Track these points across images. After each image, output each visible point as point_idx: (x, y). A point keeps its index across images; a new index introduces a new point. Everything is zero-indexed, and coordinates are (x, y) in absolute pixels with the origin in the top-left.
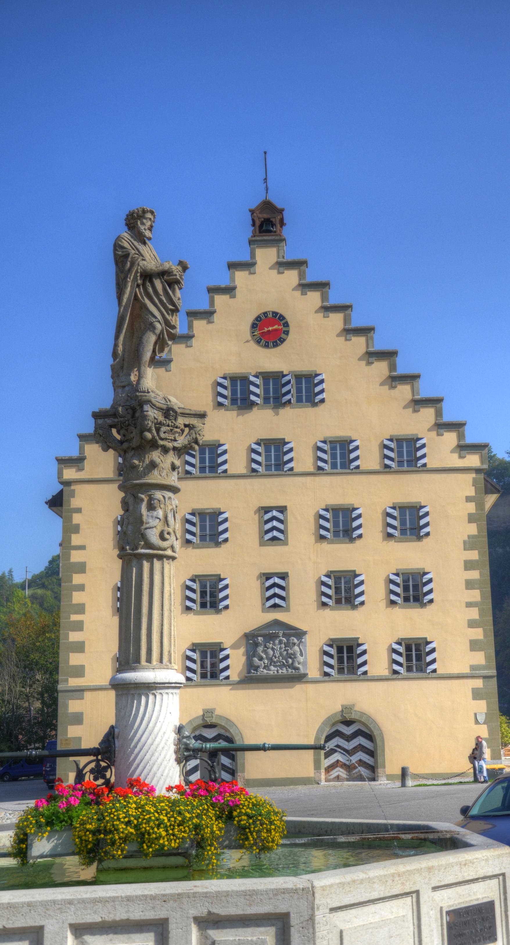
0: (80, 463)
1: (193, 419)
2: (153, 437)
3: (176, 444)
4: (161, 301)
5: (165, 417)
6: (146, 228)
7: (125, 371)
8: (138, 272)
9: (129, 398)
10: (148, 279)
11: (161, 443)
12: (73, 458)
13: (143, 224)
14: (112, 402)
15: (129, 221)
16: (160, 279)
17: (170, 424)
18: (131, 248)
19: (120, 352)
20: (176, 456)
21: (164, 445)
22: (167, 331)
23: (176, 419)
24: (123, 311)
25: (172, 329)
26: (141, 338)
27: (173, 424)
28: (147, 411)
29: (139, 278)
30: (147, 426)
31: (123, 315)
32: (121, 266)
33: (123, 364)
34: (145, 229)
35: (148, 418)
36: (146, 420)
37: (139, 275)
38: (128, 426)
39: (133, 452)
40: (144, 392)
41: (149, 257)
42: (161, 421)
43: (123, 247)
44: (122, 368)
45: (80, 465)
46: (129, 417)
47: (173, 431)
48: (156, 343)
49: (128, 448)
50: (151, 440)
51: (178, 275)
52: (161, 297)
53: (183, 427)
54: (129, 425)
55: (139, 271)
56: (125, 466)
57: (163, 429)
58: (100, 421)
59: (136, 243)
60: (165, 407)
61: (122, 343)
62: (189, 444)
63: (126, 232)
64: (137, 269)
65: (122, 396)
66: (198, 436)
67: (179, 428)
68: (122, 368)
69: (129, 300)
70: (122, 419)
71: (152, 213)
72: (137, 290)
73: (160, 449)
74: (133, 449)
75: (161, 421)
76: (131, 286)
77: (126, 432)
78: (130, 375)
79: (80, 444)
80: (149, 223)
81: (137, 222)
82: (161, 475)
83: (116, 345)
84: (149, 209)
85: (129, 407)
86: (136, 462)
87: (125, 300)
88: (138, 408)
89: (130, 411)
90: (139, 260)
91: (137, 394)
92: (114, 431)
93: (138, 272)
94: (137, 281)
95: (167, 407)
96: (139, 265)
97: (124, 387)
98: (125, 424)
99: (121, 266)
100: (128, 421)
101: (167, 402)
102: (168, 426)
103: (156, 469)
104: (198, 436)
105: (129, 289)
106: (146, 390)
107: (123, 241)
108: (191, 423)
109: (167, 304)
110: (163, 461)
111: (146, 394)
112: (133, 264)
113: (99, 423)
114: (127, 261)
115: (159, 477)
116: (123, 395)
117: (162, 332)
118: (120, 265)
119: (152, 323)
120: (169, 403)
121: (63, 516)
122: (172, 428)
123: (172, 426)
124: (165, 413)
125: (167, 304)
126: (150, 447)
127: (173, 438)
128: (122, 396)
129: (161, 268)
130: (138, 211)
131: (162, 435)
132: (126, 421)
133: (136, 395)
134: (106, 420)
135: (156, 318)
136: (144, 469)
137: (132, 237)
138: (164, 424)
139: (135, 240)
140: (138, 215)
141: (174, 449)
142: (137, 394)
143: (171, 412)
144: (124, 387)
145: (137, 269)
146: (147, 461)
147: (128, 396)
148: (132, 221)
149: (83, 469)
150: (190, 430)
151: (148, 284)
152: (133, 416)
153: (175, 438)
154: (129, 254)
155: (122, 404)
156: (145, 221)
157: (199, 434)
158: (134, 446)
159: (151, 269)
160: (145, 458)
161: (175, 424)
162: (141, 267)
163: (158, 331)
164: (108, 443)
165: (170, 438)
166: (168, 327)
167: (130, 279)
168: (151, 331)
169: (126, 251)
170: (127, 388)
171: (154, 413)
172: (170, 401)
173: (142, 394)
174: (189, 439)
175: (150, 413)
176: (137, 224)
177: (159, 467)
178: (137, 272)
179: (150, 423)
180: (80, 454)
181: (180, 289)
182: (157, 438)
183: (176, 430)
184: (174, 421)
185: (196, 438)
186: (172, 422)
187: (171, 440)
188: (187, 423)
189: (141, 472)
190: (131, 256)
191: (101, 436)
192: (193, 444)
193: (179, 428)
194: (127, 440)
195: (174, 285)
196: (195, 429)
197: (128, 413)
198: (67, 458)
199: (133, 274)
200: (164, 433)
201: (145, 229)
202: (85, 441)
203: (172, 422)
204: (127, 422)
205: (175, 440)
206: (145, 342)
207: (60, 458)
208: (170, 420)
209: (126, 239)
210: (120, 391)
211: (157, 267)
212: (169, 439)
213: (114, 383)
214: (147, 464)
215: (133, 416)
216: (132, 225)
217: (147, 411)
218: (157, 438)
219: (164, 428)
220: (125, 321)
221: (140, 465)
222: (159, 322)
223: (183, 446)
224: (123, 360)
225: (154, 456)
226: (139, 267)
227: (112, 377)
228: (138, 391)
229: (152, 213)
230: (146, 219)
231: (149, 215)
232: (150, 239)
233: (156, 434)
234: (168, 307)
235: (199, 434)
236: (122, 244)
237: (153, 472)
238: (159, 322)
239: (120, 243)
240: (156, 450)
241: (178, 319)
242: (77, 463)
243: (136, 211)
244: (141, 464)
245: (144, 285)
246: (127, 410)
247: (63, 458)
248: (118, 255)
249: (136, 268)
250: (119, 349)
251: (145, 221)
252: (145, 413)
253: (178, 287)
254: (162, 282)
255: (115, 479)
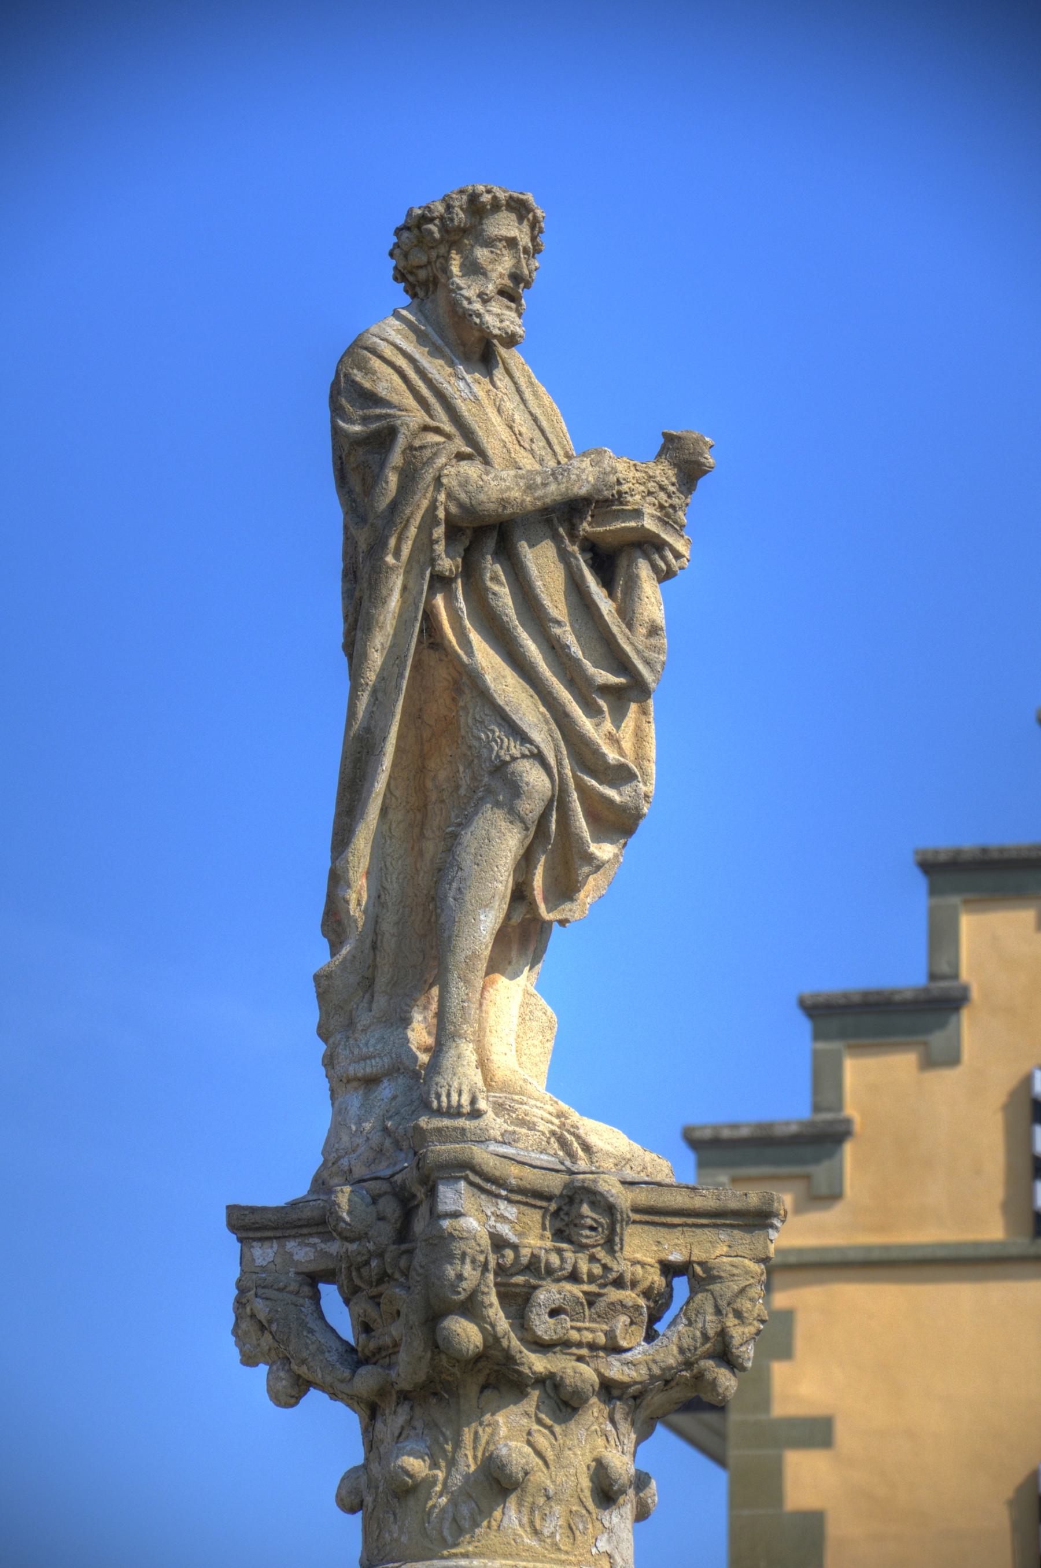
0: (817, 1160)
1: (708, 1234)
2: (492, 1340)
3: (616, 1369)
4: (554, 649)
5: (559, 1235)
6: (491, 288)
7: (381, 1001)
8: (436, 522)
9: (388, 1142)
10: (491, 544)
11: (538, 1363)
12: (780, 1131)
13: (473, 269)
14: (321, 1160)
15: (406, 255)
16: (556, 539)
17: (584, 1267)
18: (410, 401)
19: (355, 910)
20: (624, 1426)
21: (552, 1376)
22: (586, 794)
23: (610, 1244)
24: (370, 714)
25: (612, 784)
26: (455, 836)
27: (597, 1270)
28: (456, 1215)
29: (440, 548)
30: (454, 1288)
31: (368, 730)
32: (358, 489)
33: (374, 966)
34: (484, 298)
35: (458, 1247)
36: (450, 1257)
37: (439, 532)
38: (380, 1281)
39: (401, 1418)
40: (455, 1113)
41: (505, 434)
42: (535, 1258)
43: (371, 399)
44: (368, 984)
45: (820, 1171)
46: (384, 1233)
47: (601, 1304)
48: (525, 863)
49: (382, 1392)
50: (480, 1357)
51: (648, 510)
52: (557, 631)
53: (655, 1278)
54: (384, 1277)
55: (441, 514)
56: (372, 1484)
57: (548, 1294)
58: (263, 1254)
59: (437, 369)
60: (555, 1183)
61: (365, 863)
62: (688, 1365)
63: (396, 315)
64: (433, 506)
65: (360, 1131)
66: (731, 1321)
67: (634, 1284)
68: (368, 984)
69: (395, 656)
70: (353, 1247)
71: (520, 208)
72: (440, 601)
73: (535, 1394)
74: (404, 1396)
75: (535, 1258)
76: (405, 588)
77: (373, 1313)
78: (406, 1022)
79: (816, 1055)
80: (503, 266)
81: (447, 259)
82: (536, 1532)
83: (337, 879)
84: (502, 196)
85: (385, 1186)
86: (416, 1465)
87: (376, 658)
88: (420, 1193)
89: (390, 1207)
90: (441, 460)
91: (423, 1122)
92: (330, 1295)
93: (436, 522)
94: (433, 561)
95: (566, 1186)
96: (438, 481)
97: (371, 1082)
98: (365, 1271)
99: (358, 489)
100: (381, 1255)
101: (572, 1155)
102: (574, 1277)
103: (512, 1502)
104: (731, 1321)
105: (394, 602)
106: (465, 1100)
107: (376, 363)
108: (698, 1255)
109: (587, 664)
110: (550, 1455)
111: (461, 1122)
112: (409, 477)
113: (259, 1262)
114: (383, 464)
115: (529, 1541)
116: (367, 1126)
117: (559, 800)
118: (355, 481)
119: (505, 764)
120: (583, 1164)
121: (731, 1461)
122: (593, 1288)
123: (592, 1278)
124: (556, 1214)
125: (587, 664)
126: (484, 1388)
127: (602, 1339)
128: (360, 1131)
129: (553, 487)
130: (449, 208)
131: (544, 1326)
132: (371, 1254)
133: (417, 1128)
134: (291, 1245)
135: (523, 738)
136: (454, 1502)
137: (422, 338)
138: (550, 1271)
139: (436, 352)
140: (444, 229)
141: (609, 1390)
142: (423, 1122)
143: (585, 1209)
144: (371, 1082)
145: (433, 506)
146: (469, 1462)
147: (385, 1129)
148: (419, 258)
149: (833, 1196)
150: (693, 1292)
151: (493, 570)
152: (403, 1234)
153: (610, 1335)
154: (391, 433)
155: (359, 1171)
156: (482, 254)
157: (738, 1314)
158: (405, 1385)
159: (504, 502)
160: (458, 1444)
161: (605, 1267)
162: (449, 496)
163: (531, 807)
164: (294, 1367)
165: (588, 1337)
166: (593, 774)
167: (397, 554)
168: (498, 805)
169: (379, 417)
170: (386, 1090)
171: (501, 1218)
172: (587, 1148)
173: (446, 1122)
174: (686, 1342)
175: (471, 1223)
176: (446, 270)
177: (531, 1488)
178: (430, 519)
179: (468, 1270)
180: (817, 1108)
181: (664, 576)
182: (515, 1343)
183: (614, 1295)
184: (601, 1254)
185: (723, 1334)
186: (593, 1259)
187: (593, 1347)
188: (676, 1257)
189: (441, 1519)
190: (401, 442)
191: (262, 1328)
192: (710, 1363)
193: (634, 1284)
194: (380, 1349)
195: (632, 563)
196: (716, 1287)
197: (381, 1218)
198: (744, 1132)
199: (413, 531)
200: (554, 1313)
201: (484, 298)
202: (842, 1034)
203: (593, 1259)
204: (374, 1263)
205: (612, 1348)
206: (466, 859)
207: (707, 1134)
208: (581, 1247)
209: (388, 352)
210: (354, 1100)
211: (530, 488)
212: (579, 1345)
213: (329, 1061)
214: (467, 1477)
215: (403, 1234)
216: (422, 274)
217: (456, 1215)
218: (515, 1343)
219: (554, 1288)
220: (379, 762)
221: (434, 1481)
222: (539, 757)
223: (653, 1378)
224: (374, 947)
225: (503, 1431)
226: (442, 497)
227: (324, 1033)
228: (426, 1107)
229: (520, 208)
230: (489, 243)
231: (505, 225)
232: (511, 340)
233: (503, 1324)
234: (588, 680)
235: (738, 1314)
236: (367, 385)
237: (497, 1514)
238: (539, 757)
239: (358, 376)
240: (515, 1403)
241: (651, 731)
242: (801, 1161)
243: (440, 208)
244: (441, 1475)
245: (470, 572)
246: (375, 1200)
247: (726, 1133)
248: (346, 434)
249: (425, 503)
250: (353, 897)
251: (482, 254)
252: (446, 1223)
253: (654, 567)
254: (564, 556)
255: (1014, 1251)
